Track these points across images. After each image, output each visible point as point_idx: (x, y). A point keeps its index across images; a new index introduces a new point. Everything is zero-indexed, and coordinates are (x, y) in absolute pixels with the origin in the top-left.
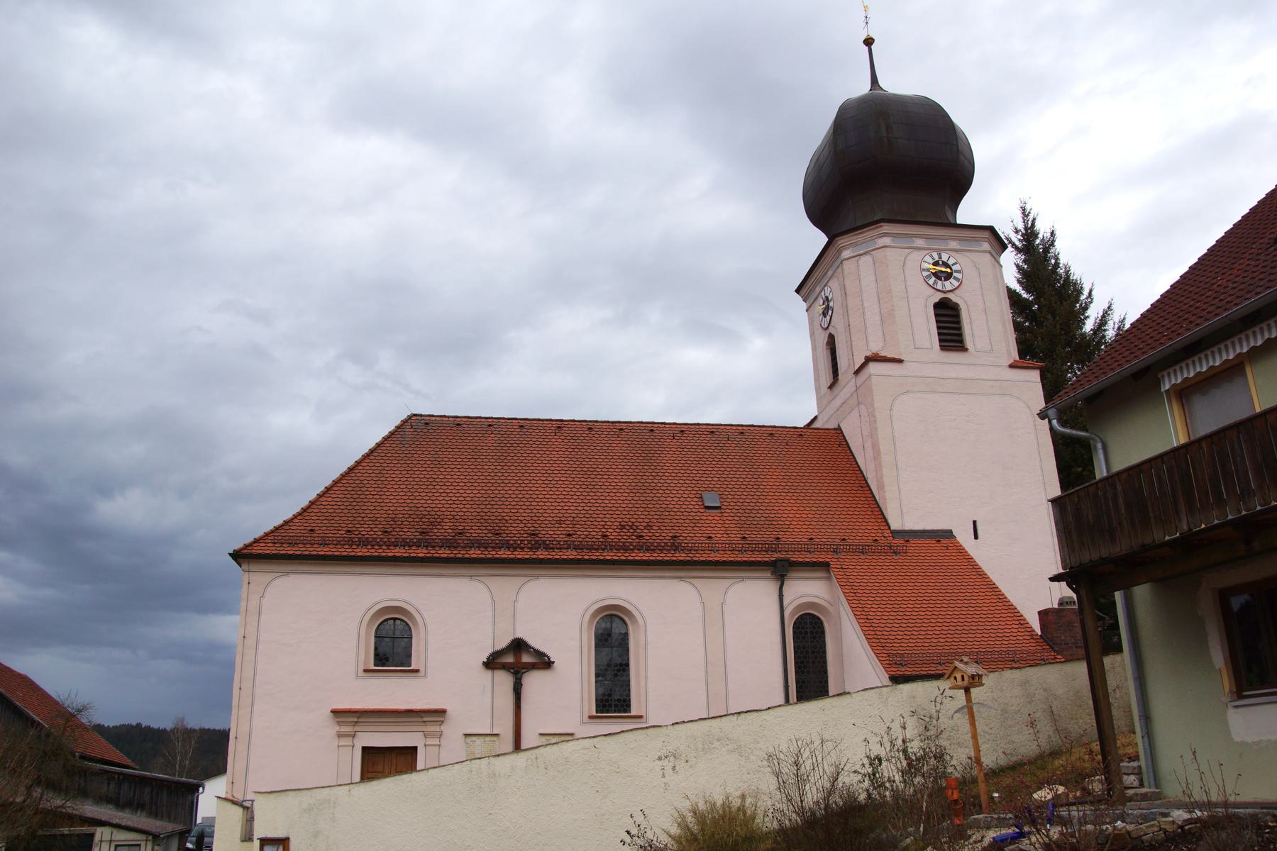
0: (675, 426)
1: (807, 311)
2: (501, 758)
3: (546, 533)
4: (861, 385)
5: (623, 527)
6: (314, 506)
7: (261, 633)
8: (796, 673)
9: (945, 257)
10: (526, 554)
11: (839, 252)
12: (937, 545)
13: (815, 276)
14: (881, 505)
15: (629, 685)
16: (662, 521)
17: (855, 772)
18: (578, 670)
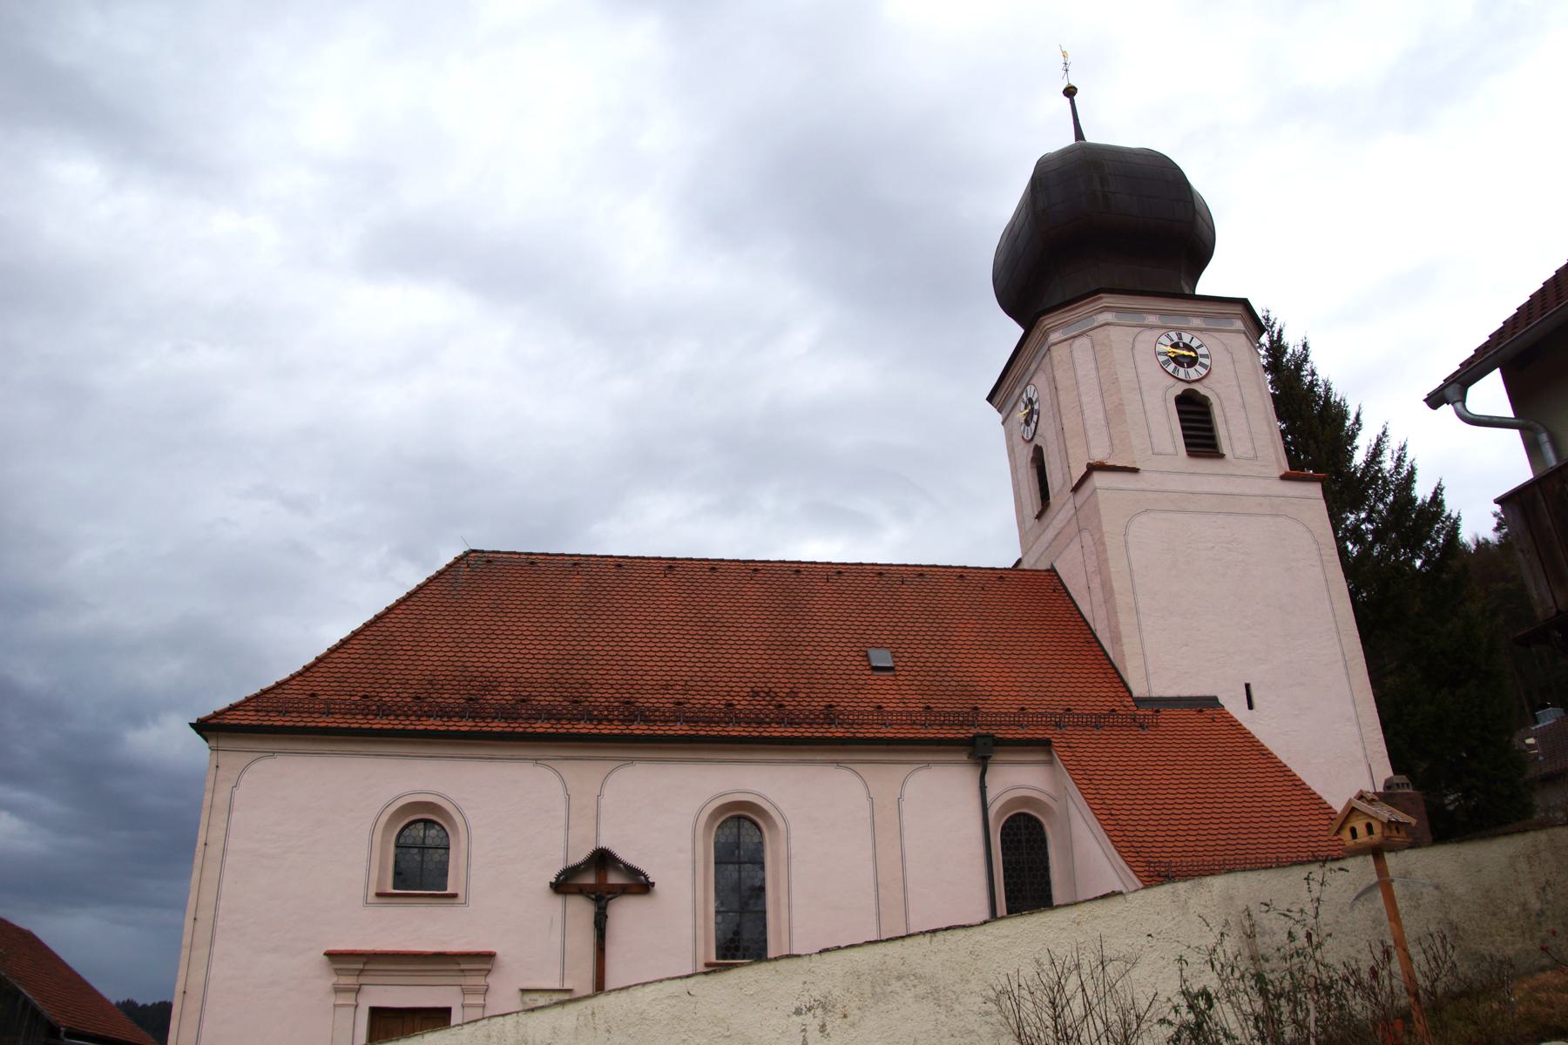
0: (830, 566)
1: (1003, 423)
2: (537, 1014)
3: (644, 701)
4: (1082, 506)
5: (757, 694)
6: (321, 664)
7: (231, 839)
8: (1008, 899)
9: (1186, 338)
10: (617, 729)
11: (1046, 335)
12: (1197, 716)
13: (1014, 372)
14: (1117, 665)
15: (765, 919)
16: (811, 686)
17: (1162, 1021)
18: (689, 896)
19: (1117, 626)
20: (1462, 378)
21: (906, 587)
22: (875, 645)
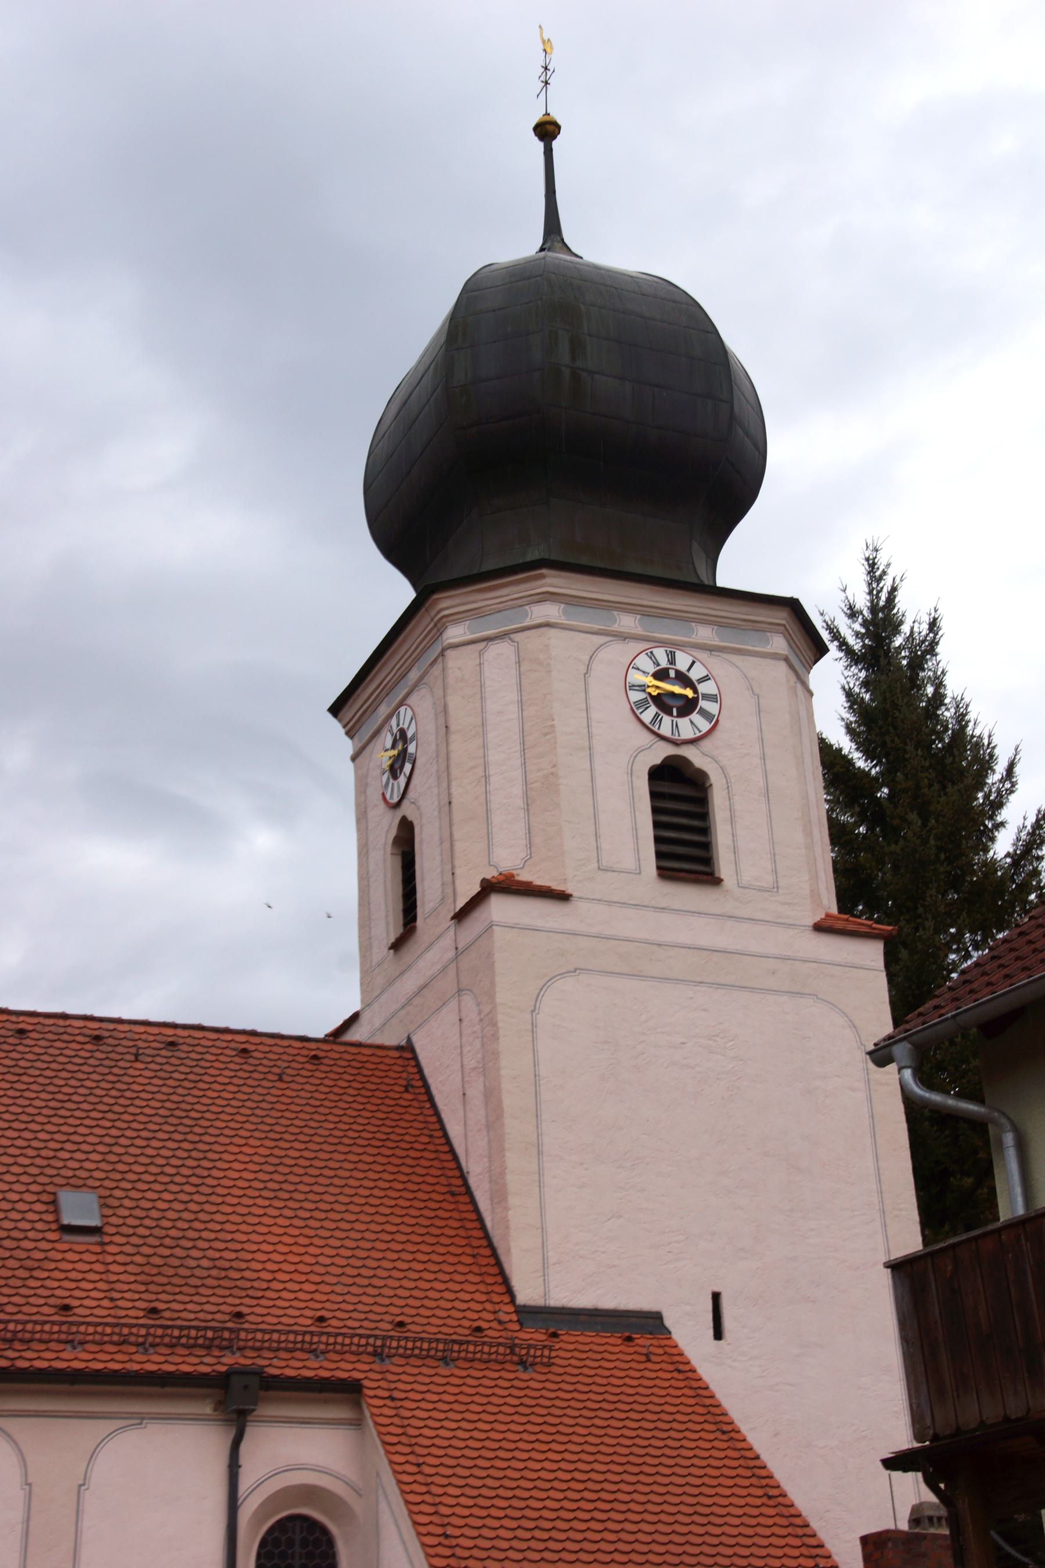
1: (354, 759)
9: (683, 662)
11: (439, 627)
19: (502, 1174)
20: (914, 1038)
21: (142, 1066)
22: (72, 1181)
